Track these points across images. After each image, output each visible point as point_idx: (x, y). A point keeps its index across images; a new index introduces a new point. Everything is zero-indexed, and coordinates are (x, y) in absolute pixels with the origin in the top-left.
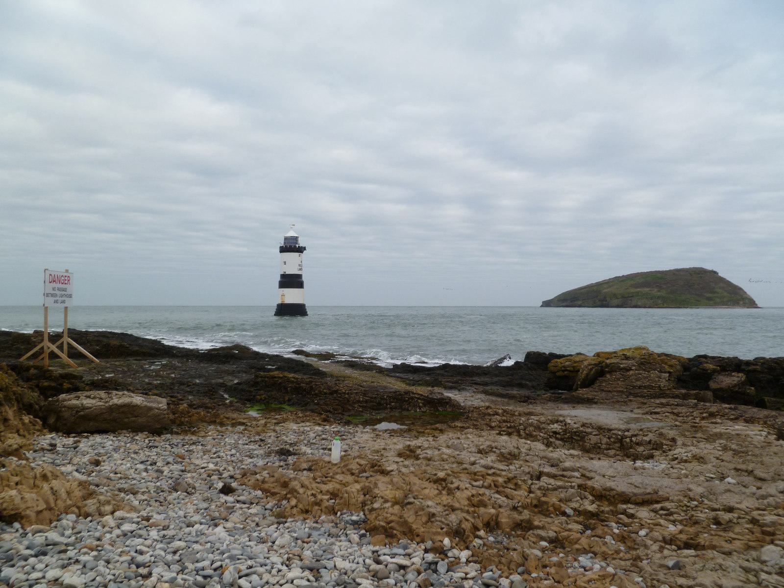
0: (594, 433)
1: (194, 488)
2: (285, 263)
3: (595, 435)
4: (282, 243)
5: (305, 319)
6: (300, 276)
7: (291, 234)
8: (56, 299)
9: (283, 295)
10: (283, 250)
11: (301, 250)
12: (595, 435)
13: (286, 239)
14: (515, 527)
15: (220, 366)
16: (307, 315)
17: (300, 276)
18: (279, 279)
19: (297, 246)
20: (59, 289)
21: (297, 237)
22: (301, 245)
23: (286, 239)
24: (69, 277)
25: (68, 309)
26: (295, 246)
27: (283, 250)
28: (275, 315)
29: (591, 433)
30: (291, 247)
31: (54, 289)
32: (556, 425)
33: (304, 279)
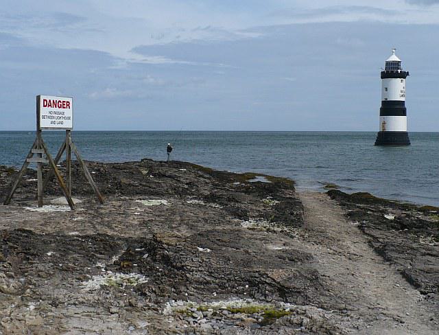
1: (127, 310)
5: (408, 148)
7: (394, 58)
8: (53, 120)
9: (384, 123)
10: (385, 75)
11: (403, 75)
13: (388, 63)
16: (376, 144)
19: (399, 71)
20: (55, 113)
23: (388, 63)
24: (68, 102)
27: (385, 75)
28: (376, 144)
30: (392, 72)
31: (50, 113)
32: (58, 206)
33: (406, 106)
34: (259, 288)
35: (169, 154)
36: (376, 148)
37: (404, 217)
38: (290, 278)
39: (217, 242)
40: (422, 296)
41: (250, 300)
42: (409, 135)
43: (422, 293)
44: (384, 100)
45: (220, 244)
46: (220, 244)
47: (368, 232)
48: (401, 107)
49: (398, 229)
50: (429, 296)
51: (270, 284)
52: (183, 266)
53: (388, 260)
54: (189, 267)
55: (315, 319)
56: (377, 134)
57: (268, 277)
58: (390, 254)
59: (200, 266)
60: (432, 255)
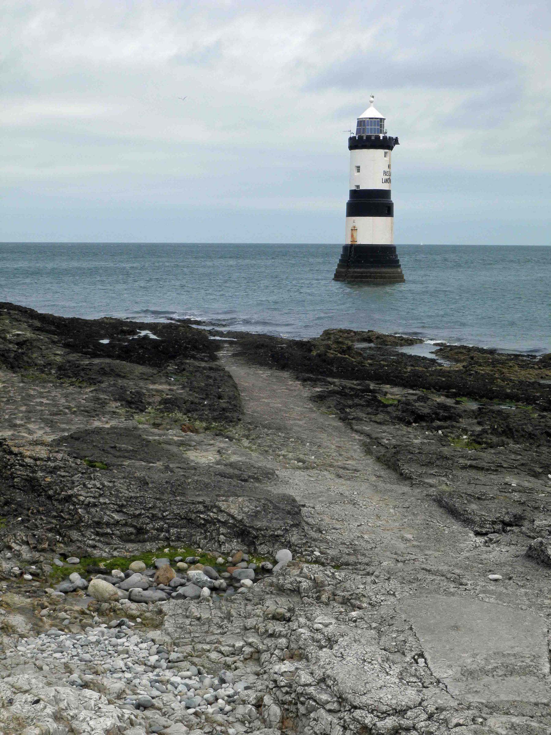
0: (328, 707)
2: (358, 170)
3: (330, 711)
4: (352, 130)
5: (403, 287)
6: (386, 194)
7: (371, 113)
9: (354, 229)
12: (330, 711)
13: (361, 123)
14: (162, 622)
15: (239, 261)
17: (386, 194)
18: (347, 198)
19: (381, 136)
21: (382, 120)
22: (388, 135)
23: (361, 123)
25: (188, 705)
26: (378, 137)
28: (338, 277)
29: (322, 705)
34: (206, 531)
35: (389, 166)
36: (336, 287)
37: (415, 401)
38: (257, 512)
39: (112, 451)
40: (480, 540)
41: (457, 369)
42: (397, 250)
43: (477, 534)
44: (354, 188)
45: (118, 454)
46: (118, 454)
47: (356, 427)
48: (383, 201)
49: (409, 424)
50: (491, 540)
51: (224, 524)
52: (70, 496)
53: (404, 478)
54: (82, 498)
55: (322, 582)
56: (341, 251)
57: (222, 511)
58: (406, 469)
59: (101, 495)
60: (481, 469)
